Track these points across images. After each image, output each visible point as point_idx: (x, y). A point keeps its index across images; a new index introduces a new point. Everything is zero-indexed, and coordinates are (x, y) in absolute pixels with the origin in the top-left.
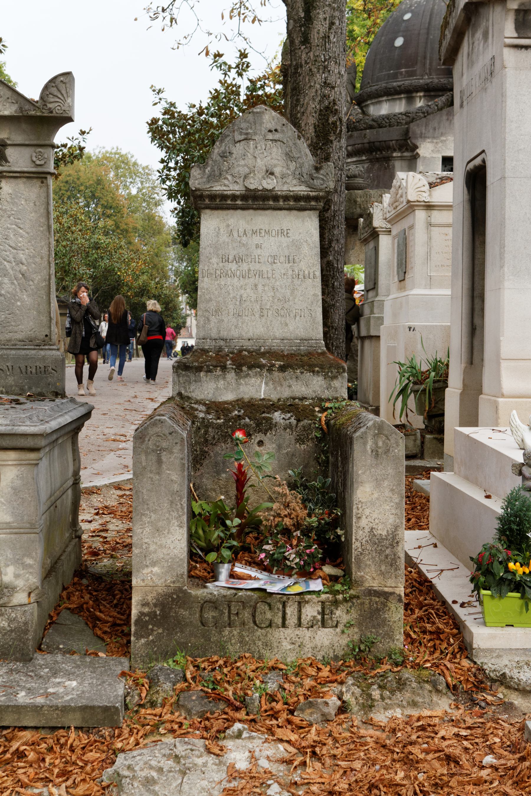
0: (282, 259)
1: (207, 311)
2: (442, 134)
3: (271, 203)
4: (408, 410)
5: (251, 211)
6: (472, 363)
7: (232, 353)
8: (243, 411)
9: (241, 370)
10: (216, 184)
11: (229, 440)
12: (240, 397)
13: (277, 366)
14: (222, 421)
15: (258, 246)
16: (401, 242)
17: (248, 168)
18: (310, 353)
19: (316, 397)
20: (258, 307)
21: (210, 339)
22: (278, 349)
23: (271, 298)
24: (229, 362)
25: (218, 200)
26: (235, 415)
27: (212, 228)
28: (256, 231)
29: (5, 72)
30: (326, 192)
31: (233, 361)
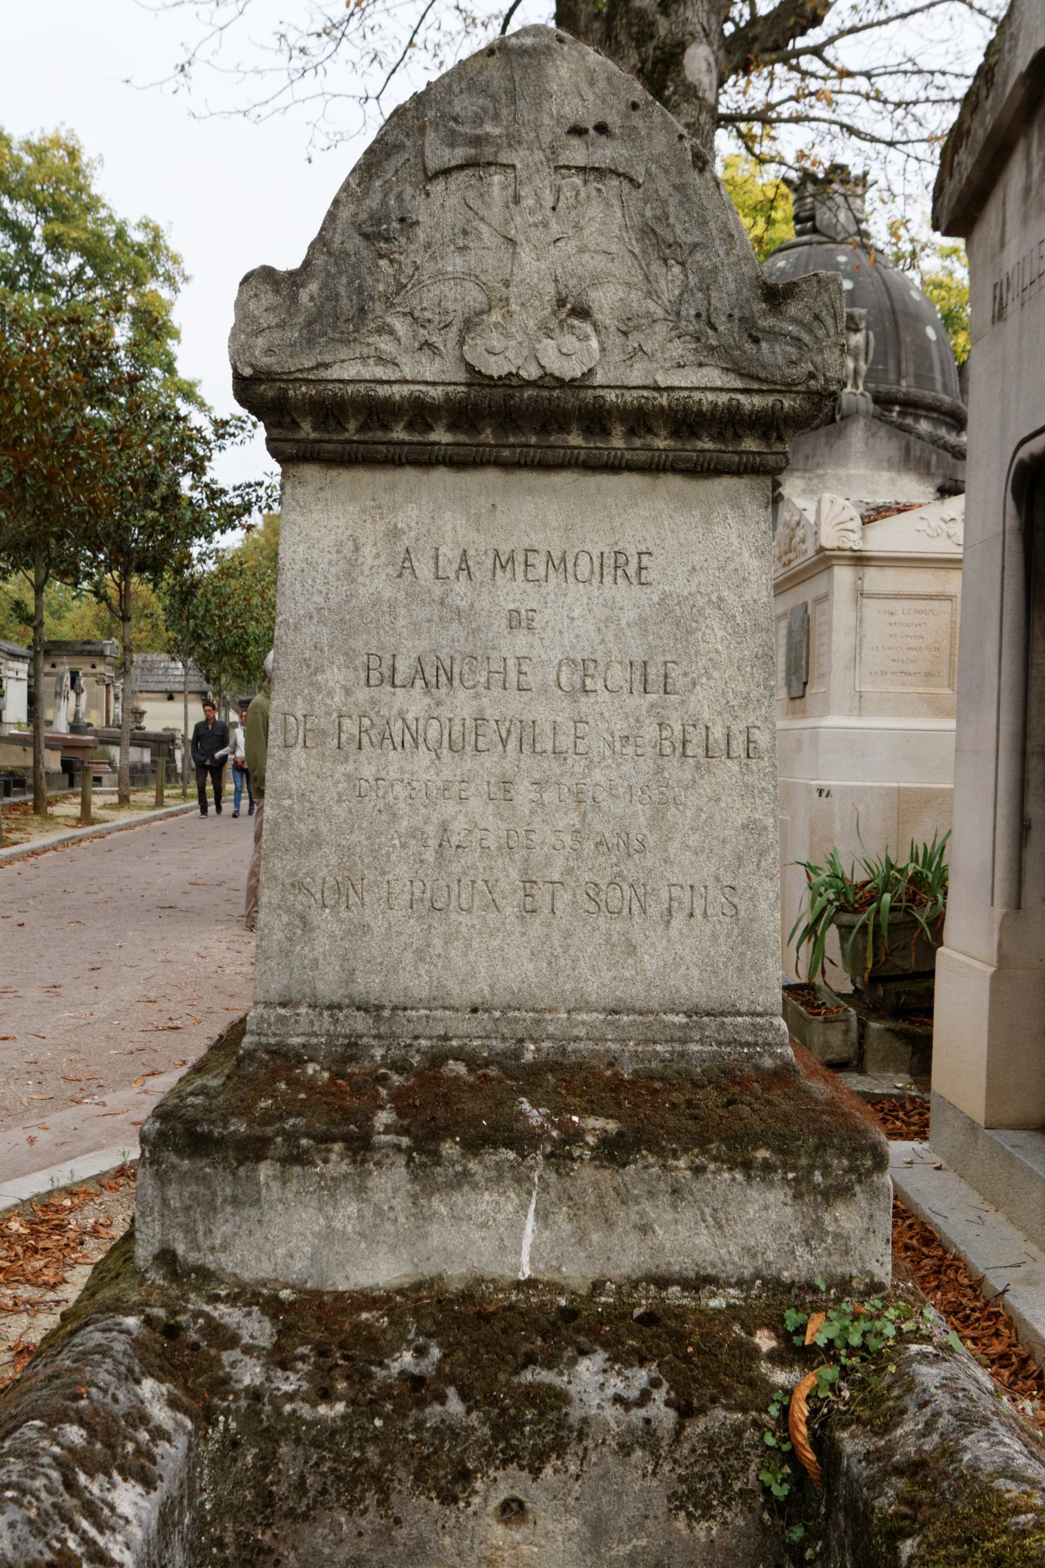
0: (618, 675)
1: (299, 886)
2: (818, 466)
3: (575, 439)
4: (826, 961)
5: (492, 476)
6: (1019, 907)
7: (401, 1067)
8: (436, 1353)
9: (437, 1158)
10: (344, 353)
11: (371, 1498)
12: (428, 1270)
13: (591, 1140)
14: (340, 1407)
15: (516, 621)
16: (796, 626)
17: (482, 286)
18: (728, 1073)
19: (757, 1275)
20: (514, 874)
21: (313, 1006)
22: (595, 1054)
23: (568, 839)
24: (384, 1118)
25: (352, 426)
26: (404, 1375)
27: (328, 541)
28: (512, 559)
29: (198, 393)
30: (809, 393)
31: (401, 1114)
